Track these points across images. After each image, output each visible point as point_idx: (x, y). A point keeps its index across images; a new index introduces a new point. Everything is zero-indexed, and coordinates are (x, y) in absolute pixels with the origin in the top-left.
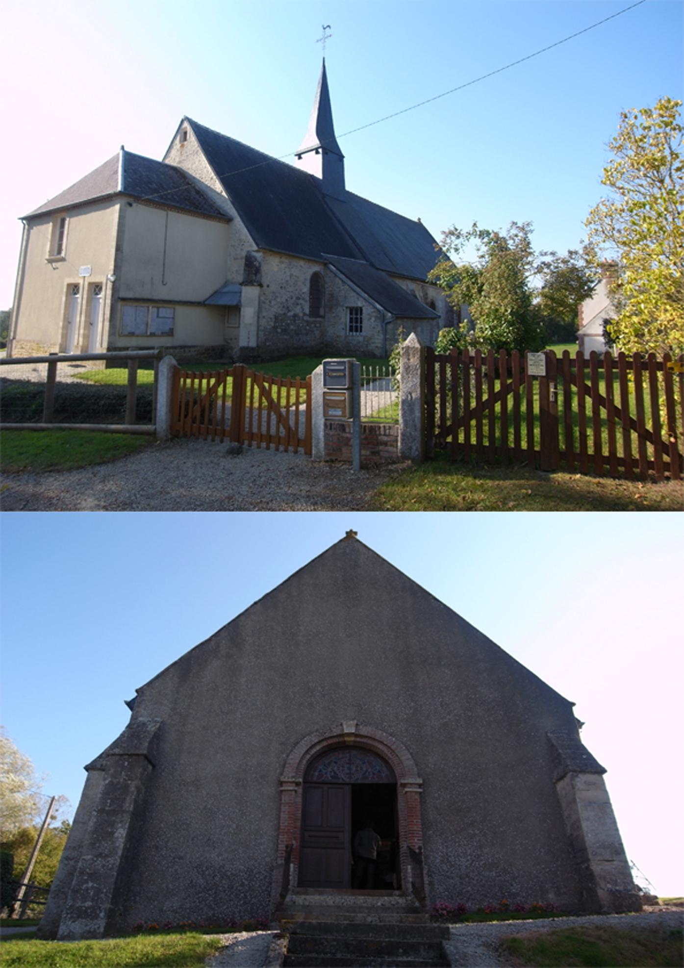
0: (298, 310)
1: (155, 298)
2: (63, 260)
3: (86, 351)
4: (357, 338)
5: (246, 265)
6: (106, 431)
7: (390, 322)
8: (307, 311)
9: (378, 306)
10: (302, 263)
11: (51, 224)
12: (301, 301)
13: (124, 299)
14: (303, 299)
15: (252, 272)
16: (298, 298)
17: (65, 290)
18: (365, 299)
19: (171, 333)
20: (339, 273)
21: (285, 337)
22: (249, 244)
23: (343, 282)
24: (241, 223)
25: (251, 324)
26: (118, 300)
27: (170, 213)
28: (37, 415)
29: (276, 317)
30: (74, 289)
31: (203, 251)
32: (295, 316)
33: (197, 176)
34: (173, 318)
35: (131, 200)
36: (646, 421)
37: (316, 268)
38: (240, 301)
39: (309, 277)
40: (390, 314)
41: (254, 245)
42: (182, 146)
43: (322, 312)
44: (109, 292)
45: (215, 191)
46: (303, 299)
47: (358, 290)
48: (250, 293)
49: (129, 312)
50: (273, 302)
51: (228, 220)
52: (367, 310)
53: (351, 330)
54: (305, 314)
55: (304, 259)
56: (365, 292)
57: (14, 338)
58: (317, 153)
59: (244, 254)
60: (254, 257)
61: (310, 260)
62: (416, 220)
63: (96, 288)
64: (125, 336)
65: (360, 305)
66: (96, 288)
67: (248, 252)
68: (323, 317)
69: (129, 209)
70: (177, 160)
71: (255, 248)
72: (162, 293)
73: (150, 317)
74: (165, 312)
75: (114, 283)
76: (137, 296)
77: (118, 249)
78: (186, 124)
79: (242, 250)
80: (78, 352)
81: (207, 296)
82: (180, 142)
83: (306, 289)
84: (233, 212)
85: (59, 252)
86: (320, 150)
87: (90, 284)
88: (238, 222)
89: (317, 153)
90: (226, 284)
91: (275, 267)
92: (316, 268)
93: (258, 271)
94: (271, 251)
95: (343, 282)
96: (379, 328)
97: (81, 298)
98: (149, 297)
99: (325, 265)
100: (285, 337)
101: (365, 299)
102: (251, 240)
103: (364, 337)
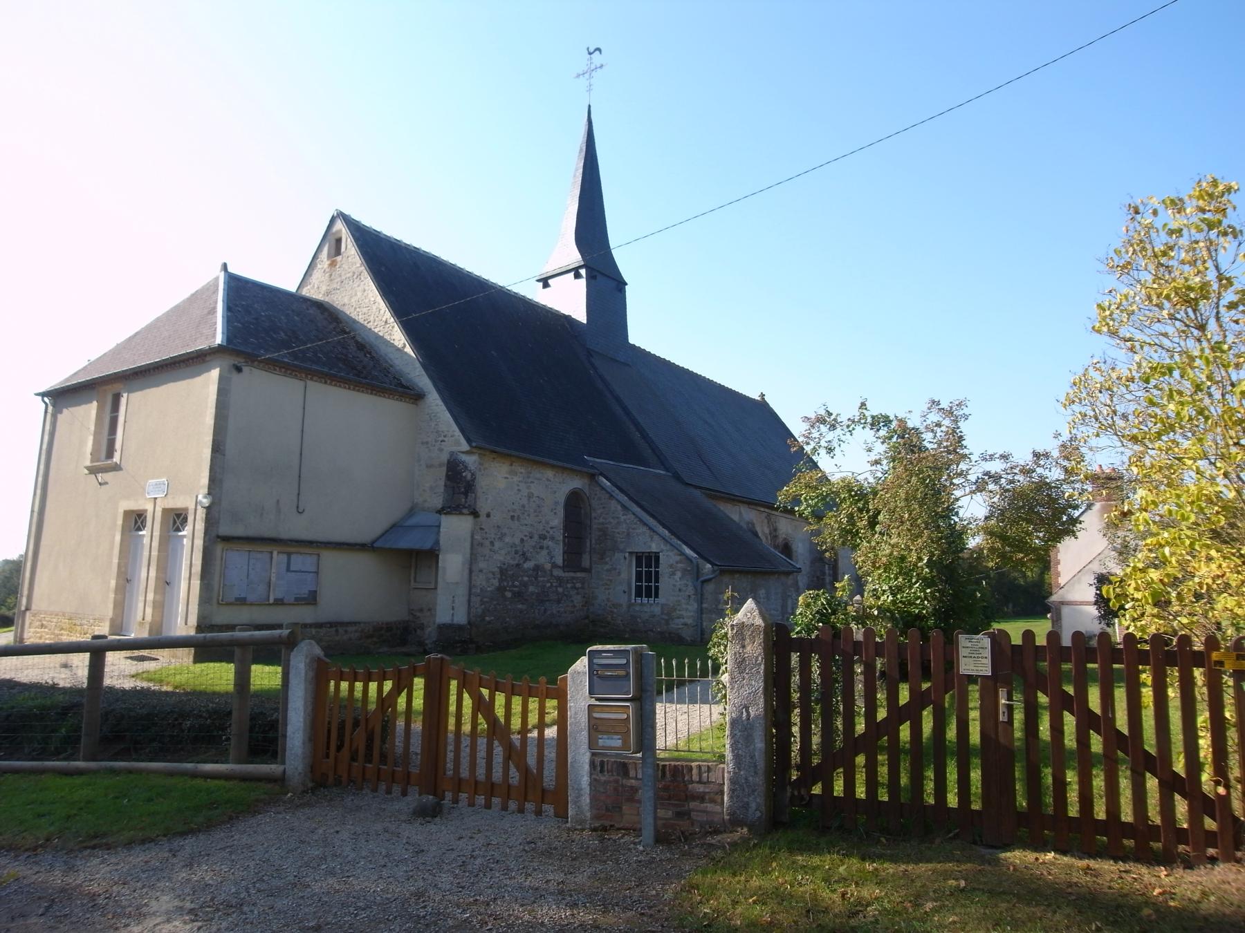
0: (542, 559)
4: (650, 608)
5: (448, 477)
6: (195, 775)
8: (559, 560)
9: (688, 551)
10: (550, 473)
13: (226, 539)
15: (459, 490)
17: (120, 522)
19: (311, 599)
22: (454, 440)
23: (624, 507)
24: (440, 402)
27: (309, 383)
28: (68, 747)
29: (503, 571)
30: (136, 520)
31: (371, 454)
32: (537, 568)
33: (360, 319)
34: (317, 573)
37: (576, 483)
38: (437, 542)
39: (562, 500)
40: (709, 566)
44: (200, 526)
45: (393, 346)
46: (552, 538)
48: (456, 528)
49: (237, 561)
50: (497, 544)
51: (414, 396)
52: (668, 559)
53: (638, 594)
54: (554, 566)
55: (553, 467)
56: (665, 526)
58: (578, 276)
59: (445, 457)
62: (755, 396)
63: (176, 519)
64: (227, 604)
66: (176, 519)
67: (452, 454)
68: (588, 570)
69: (236, 377)
70: (324, 288)
71: (465, 446)
74: (302, 561)
75: (209, 509)
76: (251, 533)
78: (340, 226)
81: (378, 531)
82: (329, 256)
83: (556, 520)
84: (423, 381)
85: (110, 454)
86: (583, 272)
87: (127, 514)
88: (434, 400)
89: (578, 276)
90: (411, 512)
91: (500, 481)
92: (576, 483)
93: (469, 487)
95: (624, 507)
96: (690, 591)
97: (150, 536)
99: (592, 477)
102: (458, 433)
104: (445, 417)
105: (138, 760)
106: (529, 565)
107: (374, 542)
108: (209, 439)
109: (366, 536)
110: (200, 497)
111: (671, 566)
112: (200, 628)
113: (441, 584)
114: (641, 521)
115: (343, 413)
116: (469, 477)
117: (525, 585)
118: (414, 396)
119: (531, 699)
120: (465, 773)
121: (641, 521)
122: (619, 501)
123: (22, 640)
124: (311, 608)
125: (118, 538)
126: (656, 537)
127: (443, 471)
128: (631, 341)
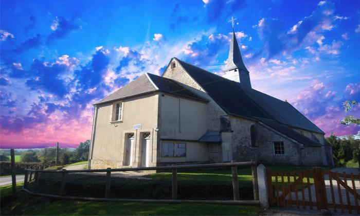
0: (246, 144)
1: (177, 139)
2: (121, 122)
3: (141, 166)
4: (280, 157)
5: (221, 122)
6: (215, 203)
7: (302, 149)
8: (251, 144)
9: (294, 141)
10: (246, 121)
11: (112, 105)
12: (248, 139)
13: (163, 140)
14: (249, 138)
15: (225, 126)
16: (246, 138)
17: (124, 136)
18: (285, 138)
19: (185, 155)
20: (265, 125)
21: (243, 157)
22: (221, 112)
23: (269, 129)
24: (213, 101)
25: (229, 151)
26: (161, 140)
27: (181, 99)
28: (169, 196)
29: (237, 147)
30: (130, 135)
31: (197, 118)
32: (245, 146)
33: (184, 83)
35: (163, 93)
36: (315, 194)
37: (253, 123)
38: (221, 140)
39: (250, 128)
40: (302, 145)
41: (224, 112)
42: (173, 70)
43: (257, 144)
44: (155, 137)
46: (249, 138)
47: (280, 133)
48: (225, 135)
49: (165, 145)
50: (235, 140)
51: (207, 102)
53: (276, 153)
54: (250, 146)
55: (246, 119)
57: (92, 159)
58: (236, 71)
59: (219, 117)
60: (224, 118)
61: (249, 119)
62: (284, 101)
63: (145, 135)
64: (164, 157)
65: (281, 140)
66: (145, 135)
67: (221, 116)
68: (258, 147)
69: (162, 97)
71: (225, 114)
72: (179, 136)
73: (177, 149)
74: (182, 145)
76: (168, 138)
77: (159, 116)
78: (174, 60)
79: (217, 115)
80: (136, 166)
81: (199, 138)
83: (249, 134)
84: (209, 98)
85: (117, 119)
86: (237, 70)
87: (126, 134)
88: (213, 102)
89: (236, 71)
90: (208, 132)
91: (235, 123)
92: (253, 123)
93: (229, 125)
94: (233, 115)
95: (269, 129)
96: (296, 151)
98: (174, 138)
99: (256, 122)
100: (243, 157)
101: (285, 138)
102: (222, 110)
103: (286, 156)
104: (217, 107)
105: (162, 199)
106: (243, 145)
107: (200, 139)
108: (157, 114)
109: (197, 139)
110: (155, 129)
111: (288, 145)
112: (158, 163)
113: (223, 151)
114: (276, 133)
115: (188, 106)
116: (228, 122)
117: (243, 151)
118: (207, 102)
119: (281, 181)
120: (337, 201)
121: (276, 133)
122: (267, 128)
123: (90, 167)
124: (184, 158)
125: (123, 140)
126: (281, 137)
127: (219, 121)
128: (252, 88)
